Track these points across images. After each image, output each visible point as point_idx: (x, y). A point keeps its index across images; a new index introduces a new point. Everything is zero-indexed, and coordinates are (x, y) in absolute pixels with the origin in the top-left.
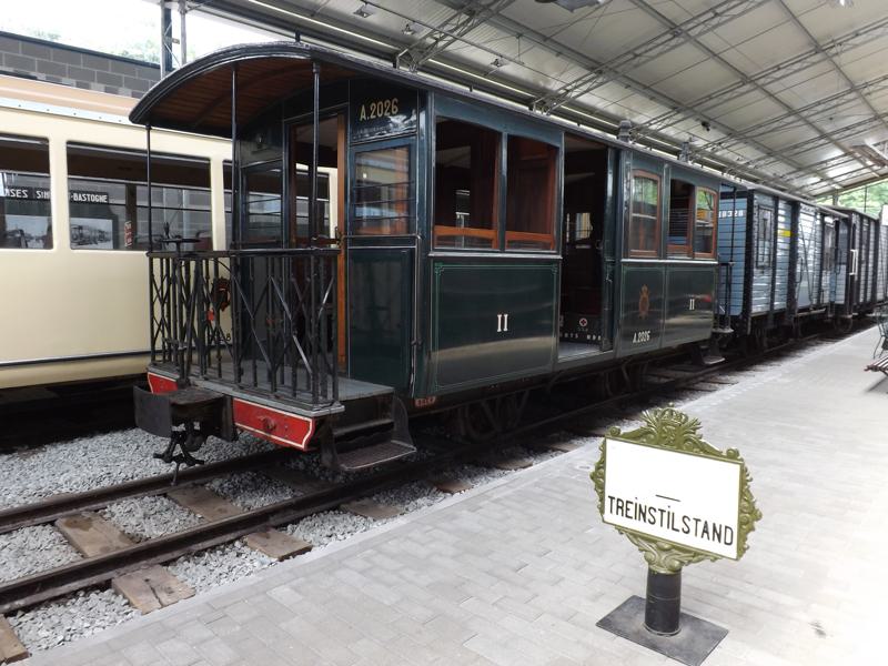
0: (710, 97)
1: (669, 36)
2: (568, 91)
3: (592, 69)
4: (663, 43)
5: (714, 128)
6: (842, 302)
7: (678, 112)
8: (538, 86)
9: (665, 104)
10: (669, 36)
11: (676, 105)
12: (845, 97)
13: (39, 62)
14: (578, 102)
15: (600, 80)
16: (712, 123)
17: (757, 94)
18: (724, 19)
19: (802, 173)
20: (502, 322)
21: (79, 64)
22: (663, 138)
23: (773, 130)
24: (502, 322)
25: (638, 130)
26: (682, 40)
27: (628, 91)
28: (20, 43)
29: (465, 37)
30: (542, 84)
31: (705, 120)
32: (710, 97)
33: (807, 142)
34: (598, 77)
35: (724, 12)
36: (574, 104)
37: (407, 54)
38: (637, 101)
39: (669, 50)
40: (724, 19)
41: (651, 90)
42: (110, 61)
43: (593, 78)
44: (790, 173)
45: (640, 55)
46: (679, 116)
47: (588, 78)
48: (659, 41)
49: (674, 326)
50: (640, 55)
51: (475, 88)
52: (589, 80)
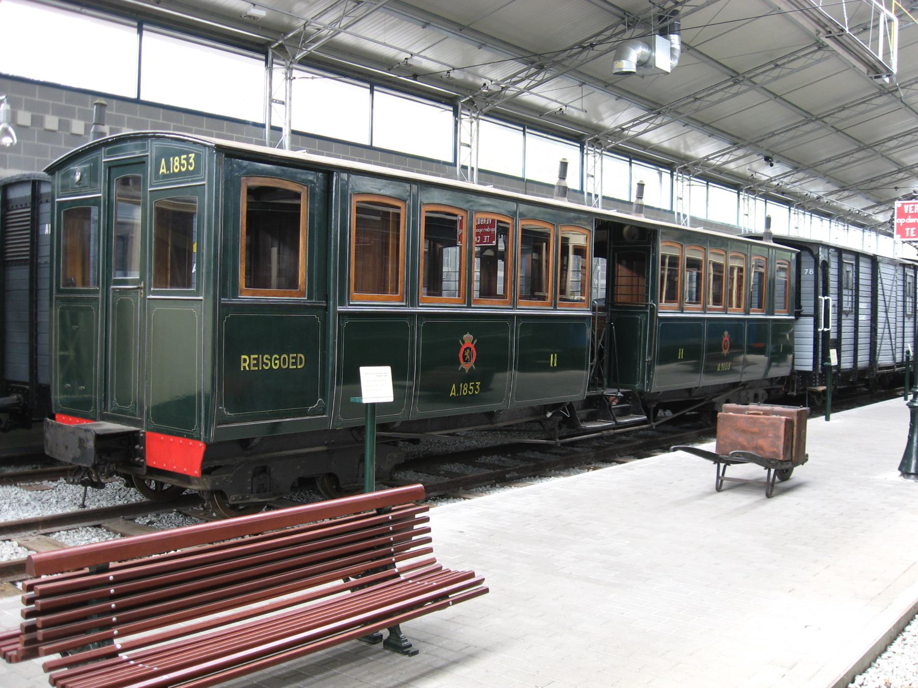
0: (773, 134)
1: (731, 83)
2: (623, 130)
3: (651, 110)
4: (722, 90)
5: (778, 162)
6: (810, 369)
7: (739, 148)
8: (591, 124)
9: (724, 140)
10: (731, 83)
11: (736, 140)
12: (874, 101)
13: (79, 110)
14: (639, 140)
15: (658, 121)
16: (775, 158)
17: (753, 96)
18: (785, 71)
19: (846, 193)
20: (553, 360)
21: (159, 118)
22: (645, 146)
23: (844, 165)
24: (553, 360)
25: (695, 165)
26: (744, 88)
27: (686, 129)
28: (161, 110)
29: (348, 30)
30: (595, 121)
31: (770, 154)
32: (773, 134)
33: (884, 176)
34: (537, 73)
35: (784, 64)
36: (514, 102)
37: (281, 46)
38: (693, 135)
39: (729, 98)
40: (785, 71)
41: (711, 129)
42: (37, 87)
43: (532, 75)
44: (831, 193)
45: (700, 99)
46: (740, 153)
47: (523, 75)
48: (718, 88)
49: (321, 445)
50: (700, 99)
51: (529, 128)
52: (527, 77)
